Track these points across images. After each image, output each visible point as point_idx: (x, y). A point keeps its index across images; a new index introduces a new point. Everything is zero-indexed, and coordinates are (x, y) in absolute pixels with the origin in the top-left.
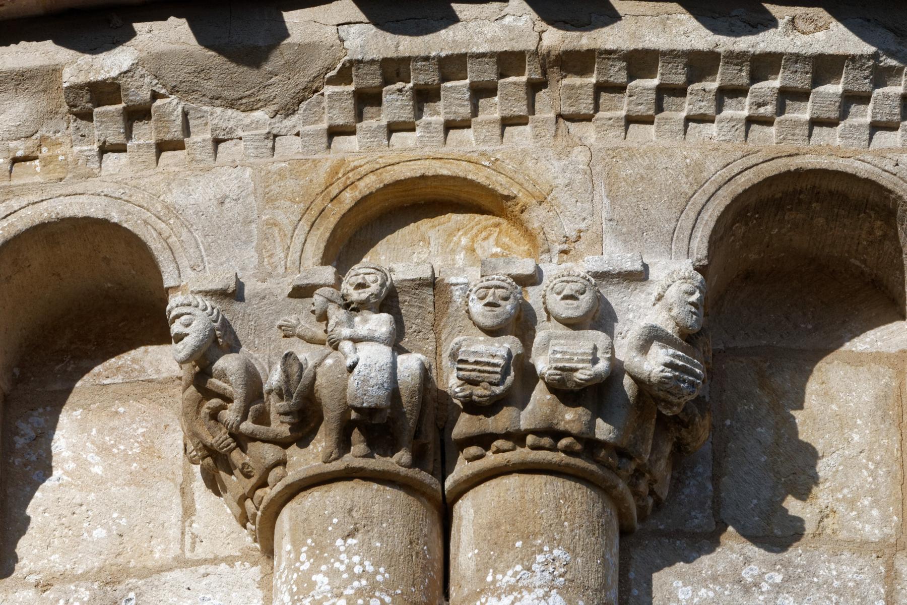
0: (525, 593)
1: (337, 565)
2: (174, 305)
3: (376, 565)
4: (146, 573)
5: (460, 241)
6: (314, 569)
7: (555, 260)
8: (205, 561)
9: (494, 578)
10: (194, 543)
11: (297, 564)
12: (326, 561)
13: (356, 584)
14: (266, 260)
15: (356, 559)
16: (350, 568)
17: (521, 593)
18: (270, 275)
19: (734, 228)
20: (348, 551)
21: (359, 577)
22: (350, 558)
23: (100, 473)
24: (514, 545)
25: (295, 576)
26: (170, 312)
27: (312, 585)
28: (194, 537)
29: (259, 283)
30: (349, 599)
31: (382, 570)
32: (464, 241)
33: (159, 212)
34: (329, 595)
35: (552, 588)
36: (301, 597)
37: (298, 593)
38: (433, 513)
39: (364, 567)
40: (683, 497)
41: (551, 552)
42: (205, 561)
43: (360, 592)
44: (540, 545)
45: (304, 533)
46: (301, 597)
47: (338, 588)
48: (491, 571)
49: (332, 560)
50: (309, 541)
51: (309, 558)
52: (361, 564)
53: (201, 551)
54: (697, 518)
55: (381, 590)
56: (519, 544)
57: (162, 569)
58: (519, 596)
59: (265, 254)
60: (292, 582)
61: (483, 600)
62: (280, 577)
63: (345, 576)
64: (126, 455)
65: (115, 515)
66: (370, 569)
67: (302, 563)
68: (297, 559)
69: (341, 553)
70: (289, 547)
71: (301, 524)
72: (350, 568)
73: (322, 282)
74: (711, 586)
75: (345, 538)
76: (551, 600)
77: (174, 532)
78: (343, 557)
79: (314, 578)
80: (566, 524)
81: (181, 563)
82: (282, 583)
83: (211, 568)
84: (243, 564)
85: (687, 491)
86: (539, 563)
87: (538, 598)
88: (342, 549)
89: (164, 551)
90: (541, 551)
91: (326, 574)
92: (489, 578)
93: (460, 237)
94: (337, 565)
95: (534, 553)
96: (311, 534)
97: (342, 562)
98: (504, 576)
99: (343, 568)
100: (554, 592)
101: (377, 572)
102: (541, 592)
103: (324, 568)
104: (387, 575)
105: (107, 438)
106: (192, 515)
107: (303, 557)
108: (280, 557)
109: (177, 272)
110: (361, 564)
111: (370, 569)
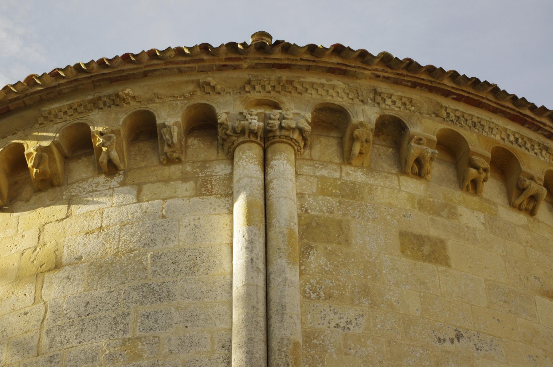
4: (210, 161)
53: (220, 158)
57: (213, 160)
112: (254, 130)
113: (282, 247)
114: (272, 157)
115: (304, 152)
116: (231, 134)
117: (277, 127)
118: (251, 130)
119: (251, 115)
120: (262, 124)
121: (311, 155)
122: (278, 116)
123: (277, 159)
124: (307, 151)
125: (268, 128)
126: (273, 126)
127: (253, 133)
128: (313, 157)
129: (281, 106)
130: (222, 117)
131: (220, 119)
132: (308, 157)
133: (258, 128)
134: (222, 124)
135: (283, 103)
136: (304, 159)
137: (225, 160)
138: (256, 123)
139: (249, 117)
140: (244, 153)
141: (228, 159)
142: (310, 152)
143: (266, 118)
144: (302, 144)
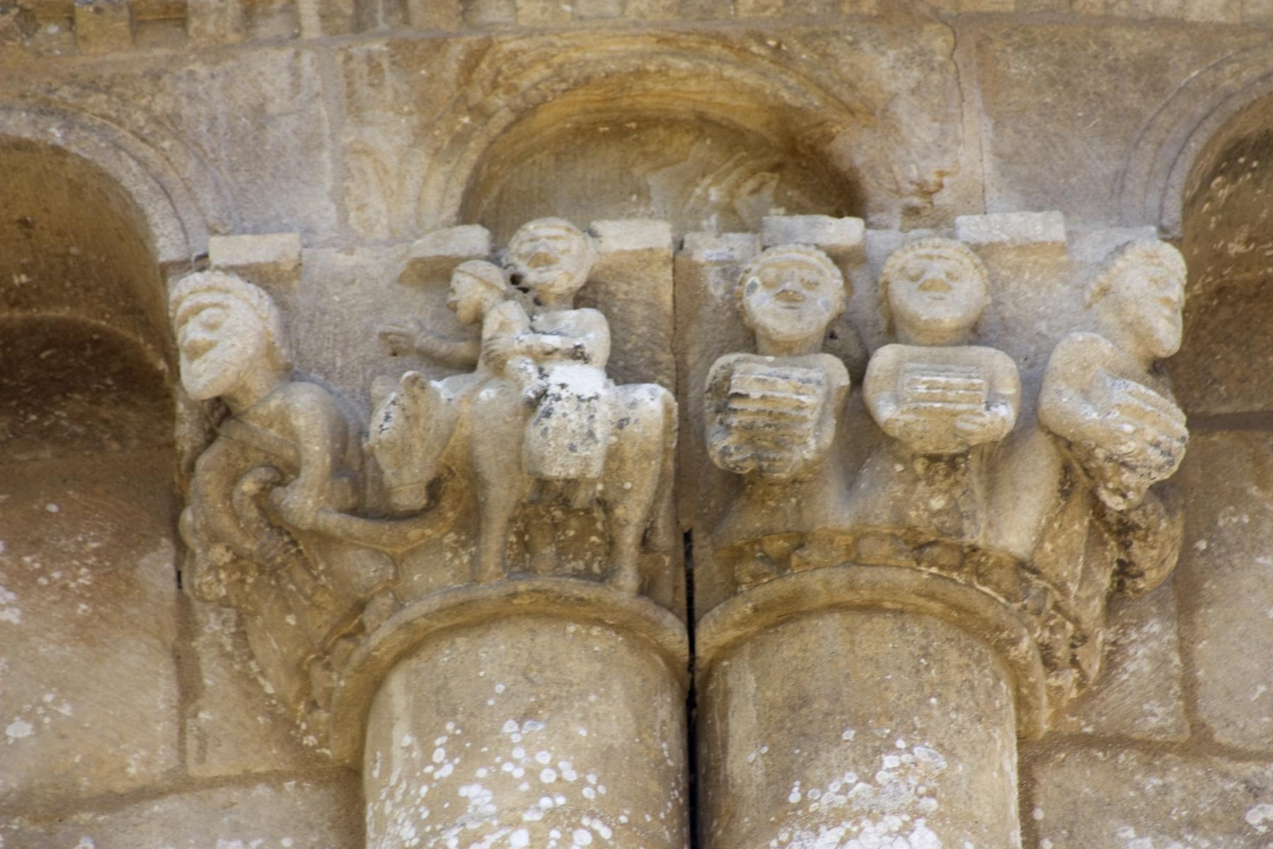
0: (865, 823)
1: (507, 767)
2: (185, 291)
3: (581, 769)
4: (112, 802)
5: (708, 195)
6: (464, 776)
7: (897, 223)
8: (228, 781)
9: (804, 795)
10: (202, 749)
11: (429, 769)
12: (485, 760)
13: (546, 802)
14: (352, 215)
15: (543, 758)
16: (533, 773)
17: (857, 823)
18: (361, 242)
19: (1213, 184)
20: (525, 744)
21: (548, 791)
22: (531, 755)
23: (16, 621)
24: (839, 737)
25: (424, 790)
26: (178, 302)
27: (460, 805)
28: (202, 738)
29: (341, 256)
30: (532, 828)
31: (592, 779)
32: (715, 195)
33: (141, 128)
34: (495, 823)
35: (916, 814)
36: (439, 827)
37: (431, 819)
38: (672, 684)
39: (559, 772)
40: (1125, 677)
41: (909, 750)
42: (228, 781)
43: (553, 816)
44: (889, 736)
45: (438, 712)
46: (439, 827)
47: (512, 810)
48: (797, 783)
49: (498, 760)
50: (450, 726)
51: (450, 757)
52: (553, 766)
53: (217, 766)
54: (1155, 715)
55: (592, 815)
56: (849, 735)
57: (144, 794)
58: (855, 829)
59: (351, 204)
60: (418, 801)
61: (784, 837)
62: (391, 796)
63: (525, 787)
64: (65, 587)
65: (48, 698)
66: (571, 776)
67: (438, 766)
68: (427, 759)
69: (513, 746)
70: (407, 740)
71: (433, 698)
72: (533, 773)
73: (464, 254)
74: (1190, 838)
75: (520, 722)
76: (914, 837)
77: (163, 728)
78: (519, 753)
79: (463, 792)
80: (933, 700)
81: (180, 784)
82: (396, 806)
83: (236, 794)
84: (298, 786)
85: (1132, 667)
86: (888, 770)
87: (890, 833)
88: (516, 738)
89: (147, 762)
90: (891, 748)
91: (485, 783)
92: (795, 797)
93: (706, 189)
94: (507, 767)
95: (877, 751)
96: (454, 712)
97: (516, 763)
98: (823, 793)
99: (519, 773)
100: (920, 823)
101: (583, 783)
102: (895, 822)
103: (482, 773)
104: (602, 790)
105: (27, 559)
106: (197, 697)
107: (439, 755)
108: (388, 760)
109: (181, 236)
110: (553, 766)
111: (571, 776)
112: (572, 483)
113: (1098, 162)
114: (782, 776)
115: (1111, 663)
116: (334, 521)
117: (814, 440)
118: (543, 484)
119: (536, 300)
120: (651, 402)
121: (1189, 687)
122: (828, 295)
123: (837, 816)
124: (1149, 644)
125: (723, 445)
126: (776, 426)
127: (556, 513)
128: (1211, 707)
129: (856, 148)
130: (220, 335)
131: (196, 352)
132: (1159, 717)
133: (613, 455)
134: (222, 412)
135: (874, 114)
136: (1116, 741)
137: (275, 779)
138: (589, 409)
139: (507, 323)
140: (473, 746)
141: (309, 767)
142: (1185, 650)
143: (679, 339)
144: (1087, 595)
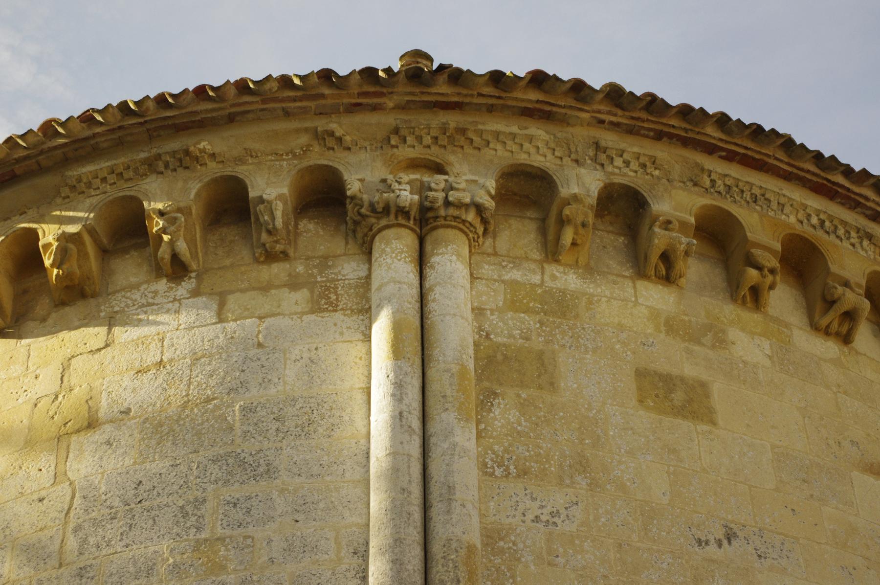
4: (334, 257)
53: (350, 252)
57: (339, 256)
112: (404, 207)
114: (433, 249)
115: (483, 243)
116: (368, 213)
117: (440, 202)
118: (399, 207)
119: (400, 183)
120: (416, 197)
121: (494, 247)
122: (442, 185)
123: (441, 254)
124: (489, 241)
125: (427, 204)
126: (434, 201)
127: (403, 212)
128: (497, 250)
129: (448, 169)
130: (353, 187)
131: (349, 189)
132: (490, 250)
133: (410, 204)
134: (353, 198)
135: (451, 164)
136: (483, 253)
137: (359, 254)
138: (407, 196)
139: (396, 186)
140: (388, 243)
141: (364, 253)
142: (494, 242)
143: (423, 188)
144: (480, 230)
